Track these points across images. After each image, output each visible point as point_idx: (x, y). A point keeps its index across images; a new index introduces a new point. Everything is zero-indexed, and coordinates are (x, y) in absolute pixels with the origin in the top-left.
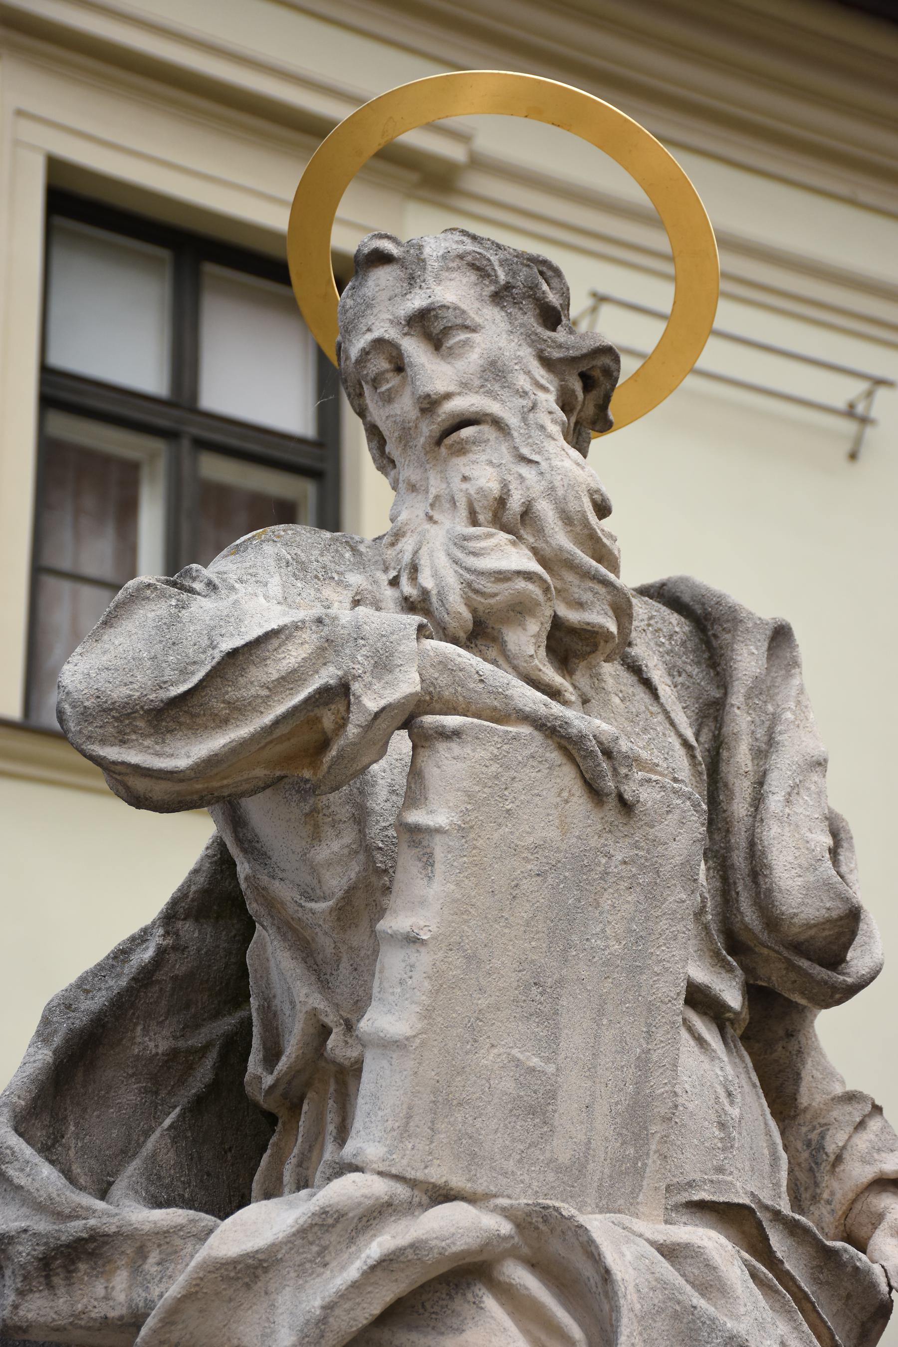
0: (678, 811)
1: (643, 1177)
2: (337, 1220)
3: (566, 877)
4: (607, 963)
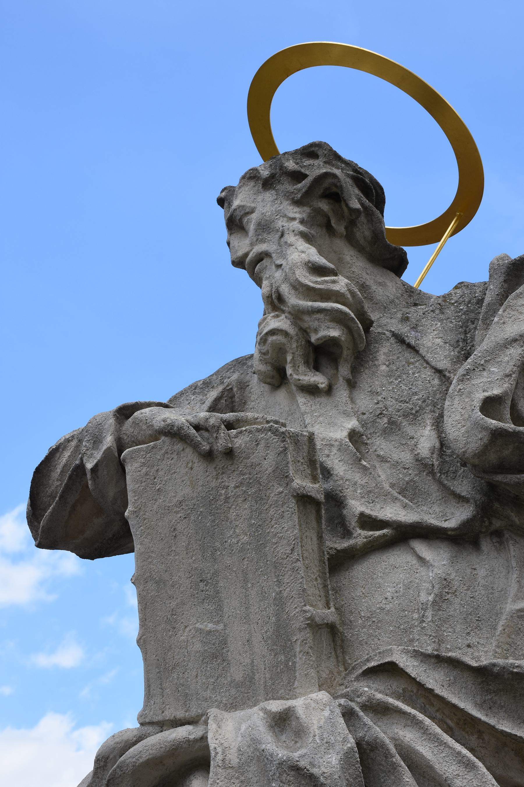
1: (295, 671)
2: (106, 762)
3: (201, 512)
4: (242, 550)
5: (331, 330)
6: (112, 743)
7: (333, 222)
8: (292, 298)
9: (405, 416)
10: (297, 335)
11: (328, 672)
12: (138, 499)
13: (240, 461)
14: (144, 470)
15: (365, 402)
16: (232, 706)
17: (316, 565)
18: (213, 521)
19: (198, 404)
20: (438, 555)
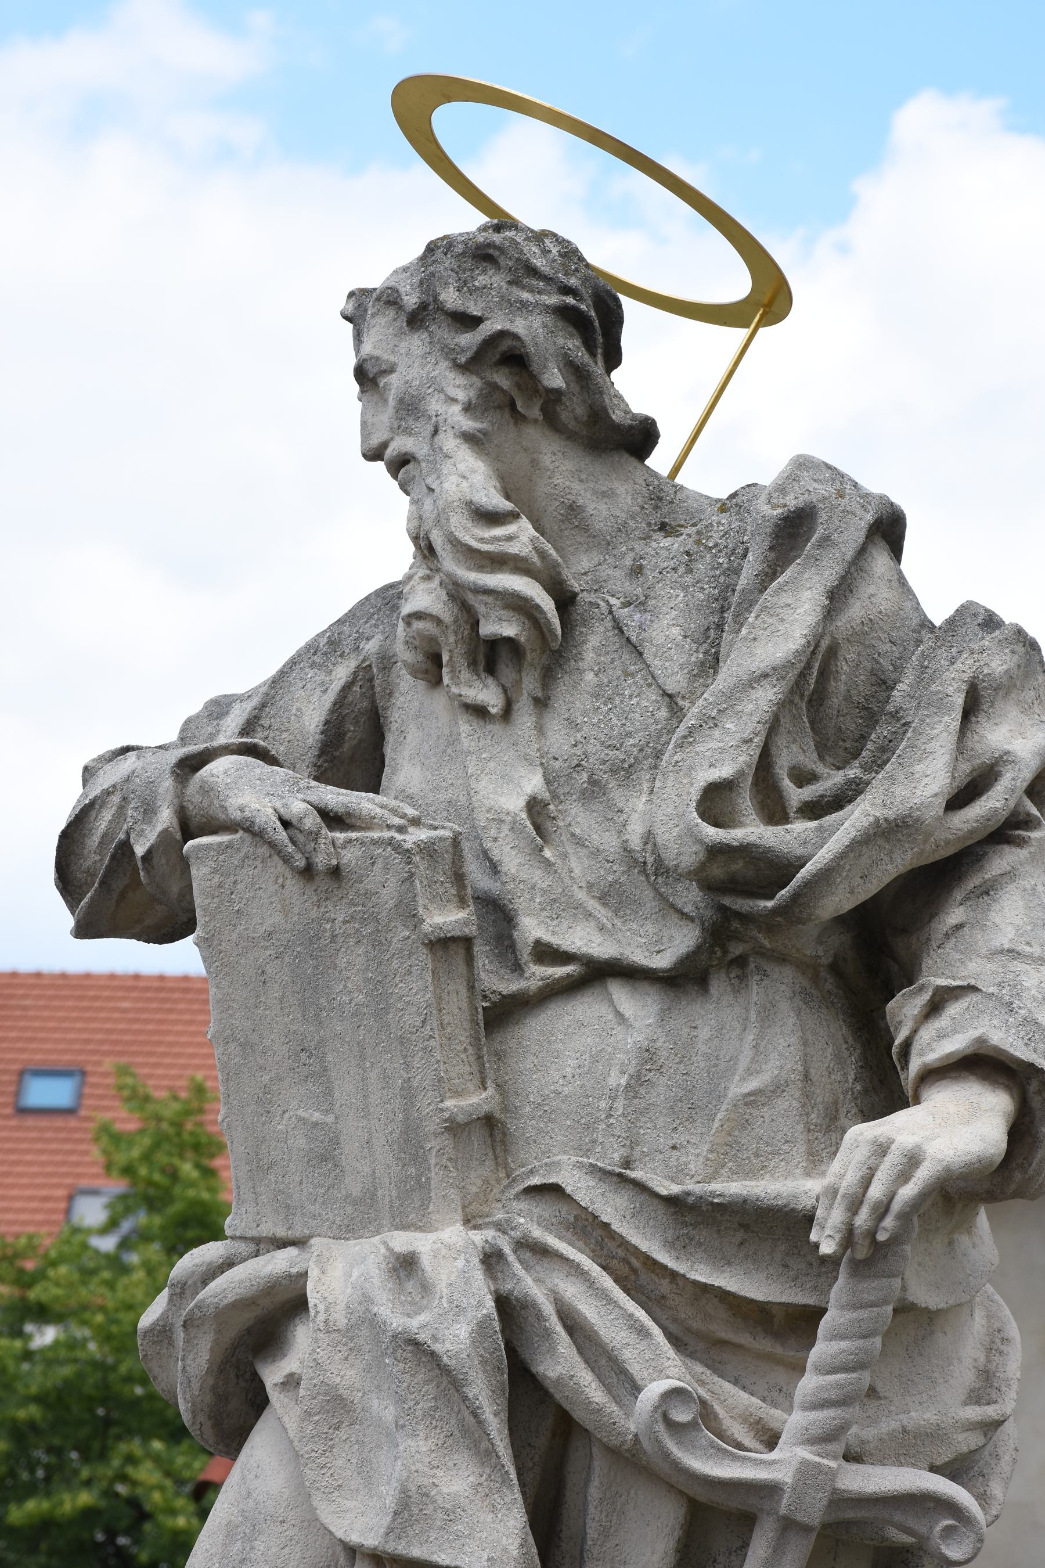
0: (381, 860)
4: (356, 1013)
5: (504, 624)
6: (190, 1265)
7: (519, 405)
8: (447, 560)
9: (614, 771)
10: (455, 621)
11: (479, 1182)
12: (210, 920)
13: (350, 884)
14: (216, 880)
15: (559, 739)
16: (347, 1231)
17: (465, 1029)
18: (316, 968)
19: (318, 692)
20: (643, 1006)
